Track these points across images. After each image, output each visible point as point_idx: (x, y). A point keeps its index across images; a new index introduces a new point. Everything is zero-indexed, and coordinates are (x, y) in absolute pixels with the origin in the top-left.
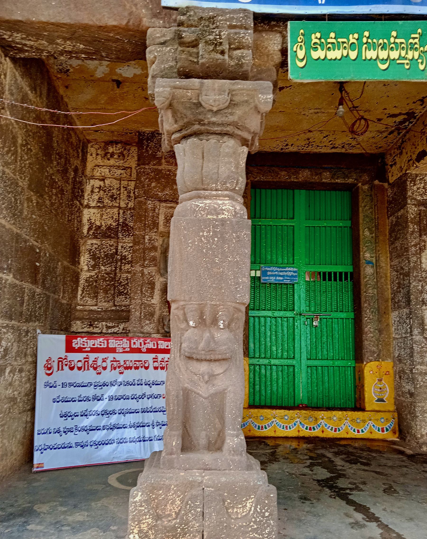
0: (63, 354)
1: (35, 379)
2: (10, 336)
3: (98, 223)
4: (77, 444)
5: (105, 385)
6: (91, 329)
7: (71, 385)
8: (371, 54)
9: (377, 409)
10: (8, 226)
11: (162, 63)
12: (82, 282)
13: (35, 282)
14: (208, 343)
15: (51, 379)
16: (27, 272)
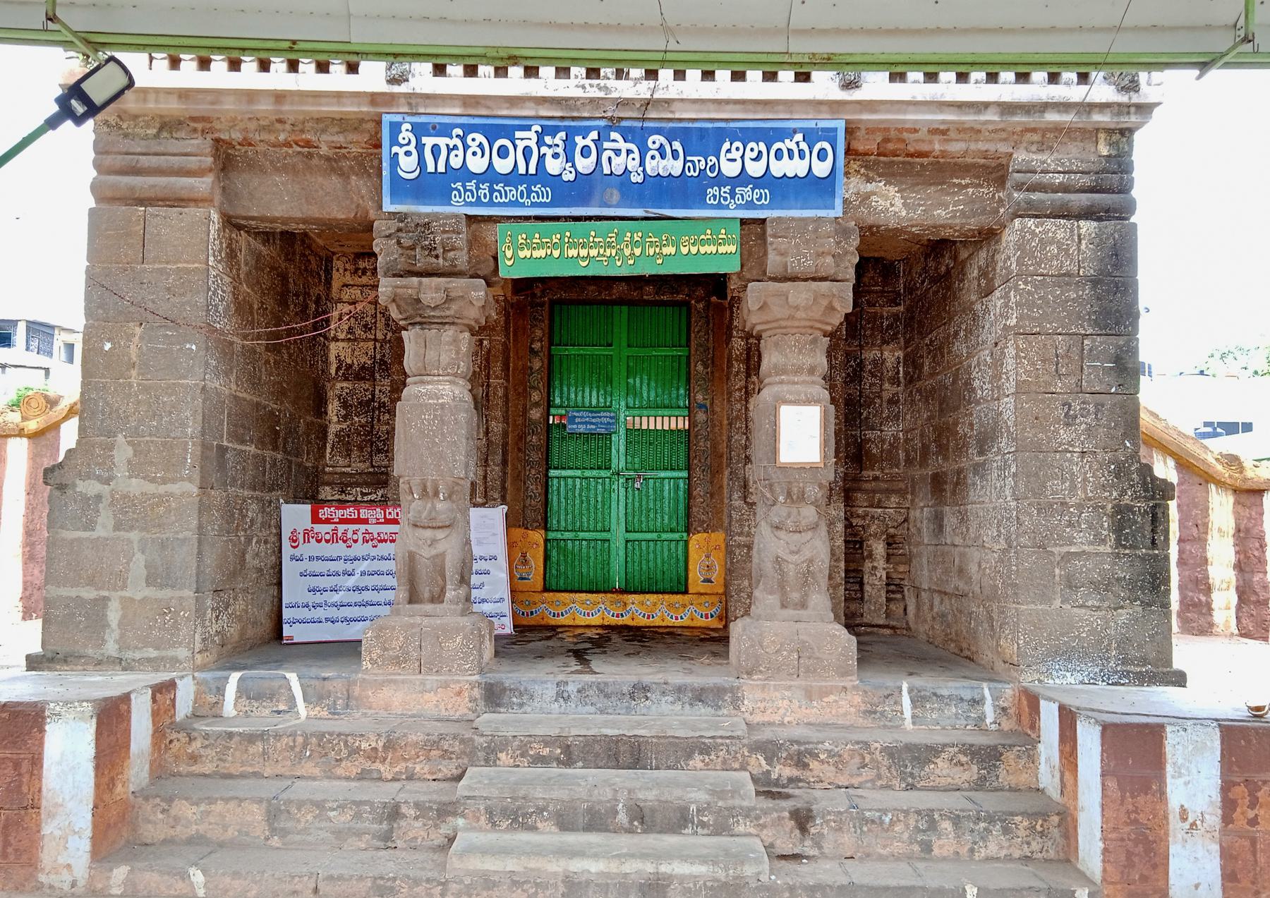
0: (309, 525)
1: (280, 552)
2: (254, 506)
3: (349, 361)
4: (327, 620)
5: (356, 559)
6: (343, 497)
7: (318, 558)
8: (573, 252)
9: (702, 591)
10: (248, 397)
11: (388, 255)
12: (331, 437)
13: (275, 448)
14: (430, 512)
15: (297, 552)
16: (267, 440)
